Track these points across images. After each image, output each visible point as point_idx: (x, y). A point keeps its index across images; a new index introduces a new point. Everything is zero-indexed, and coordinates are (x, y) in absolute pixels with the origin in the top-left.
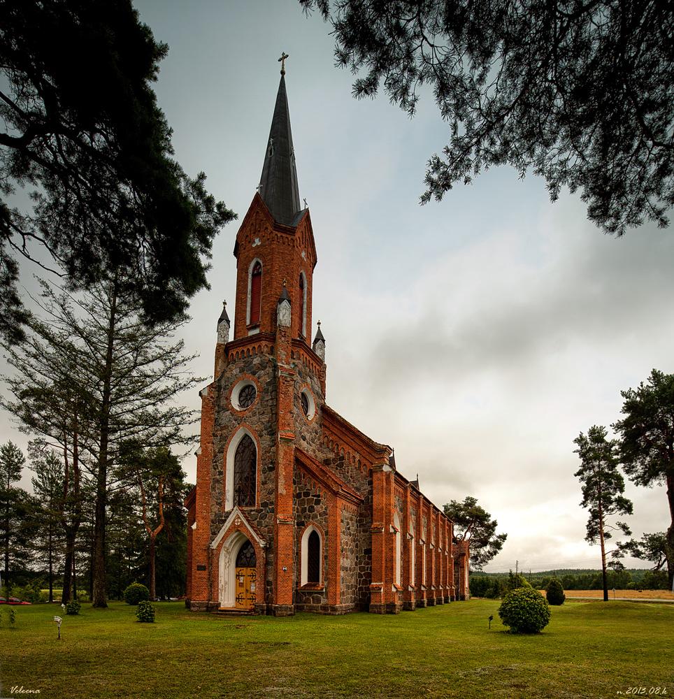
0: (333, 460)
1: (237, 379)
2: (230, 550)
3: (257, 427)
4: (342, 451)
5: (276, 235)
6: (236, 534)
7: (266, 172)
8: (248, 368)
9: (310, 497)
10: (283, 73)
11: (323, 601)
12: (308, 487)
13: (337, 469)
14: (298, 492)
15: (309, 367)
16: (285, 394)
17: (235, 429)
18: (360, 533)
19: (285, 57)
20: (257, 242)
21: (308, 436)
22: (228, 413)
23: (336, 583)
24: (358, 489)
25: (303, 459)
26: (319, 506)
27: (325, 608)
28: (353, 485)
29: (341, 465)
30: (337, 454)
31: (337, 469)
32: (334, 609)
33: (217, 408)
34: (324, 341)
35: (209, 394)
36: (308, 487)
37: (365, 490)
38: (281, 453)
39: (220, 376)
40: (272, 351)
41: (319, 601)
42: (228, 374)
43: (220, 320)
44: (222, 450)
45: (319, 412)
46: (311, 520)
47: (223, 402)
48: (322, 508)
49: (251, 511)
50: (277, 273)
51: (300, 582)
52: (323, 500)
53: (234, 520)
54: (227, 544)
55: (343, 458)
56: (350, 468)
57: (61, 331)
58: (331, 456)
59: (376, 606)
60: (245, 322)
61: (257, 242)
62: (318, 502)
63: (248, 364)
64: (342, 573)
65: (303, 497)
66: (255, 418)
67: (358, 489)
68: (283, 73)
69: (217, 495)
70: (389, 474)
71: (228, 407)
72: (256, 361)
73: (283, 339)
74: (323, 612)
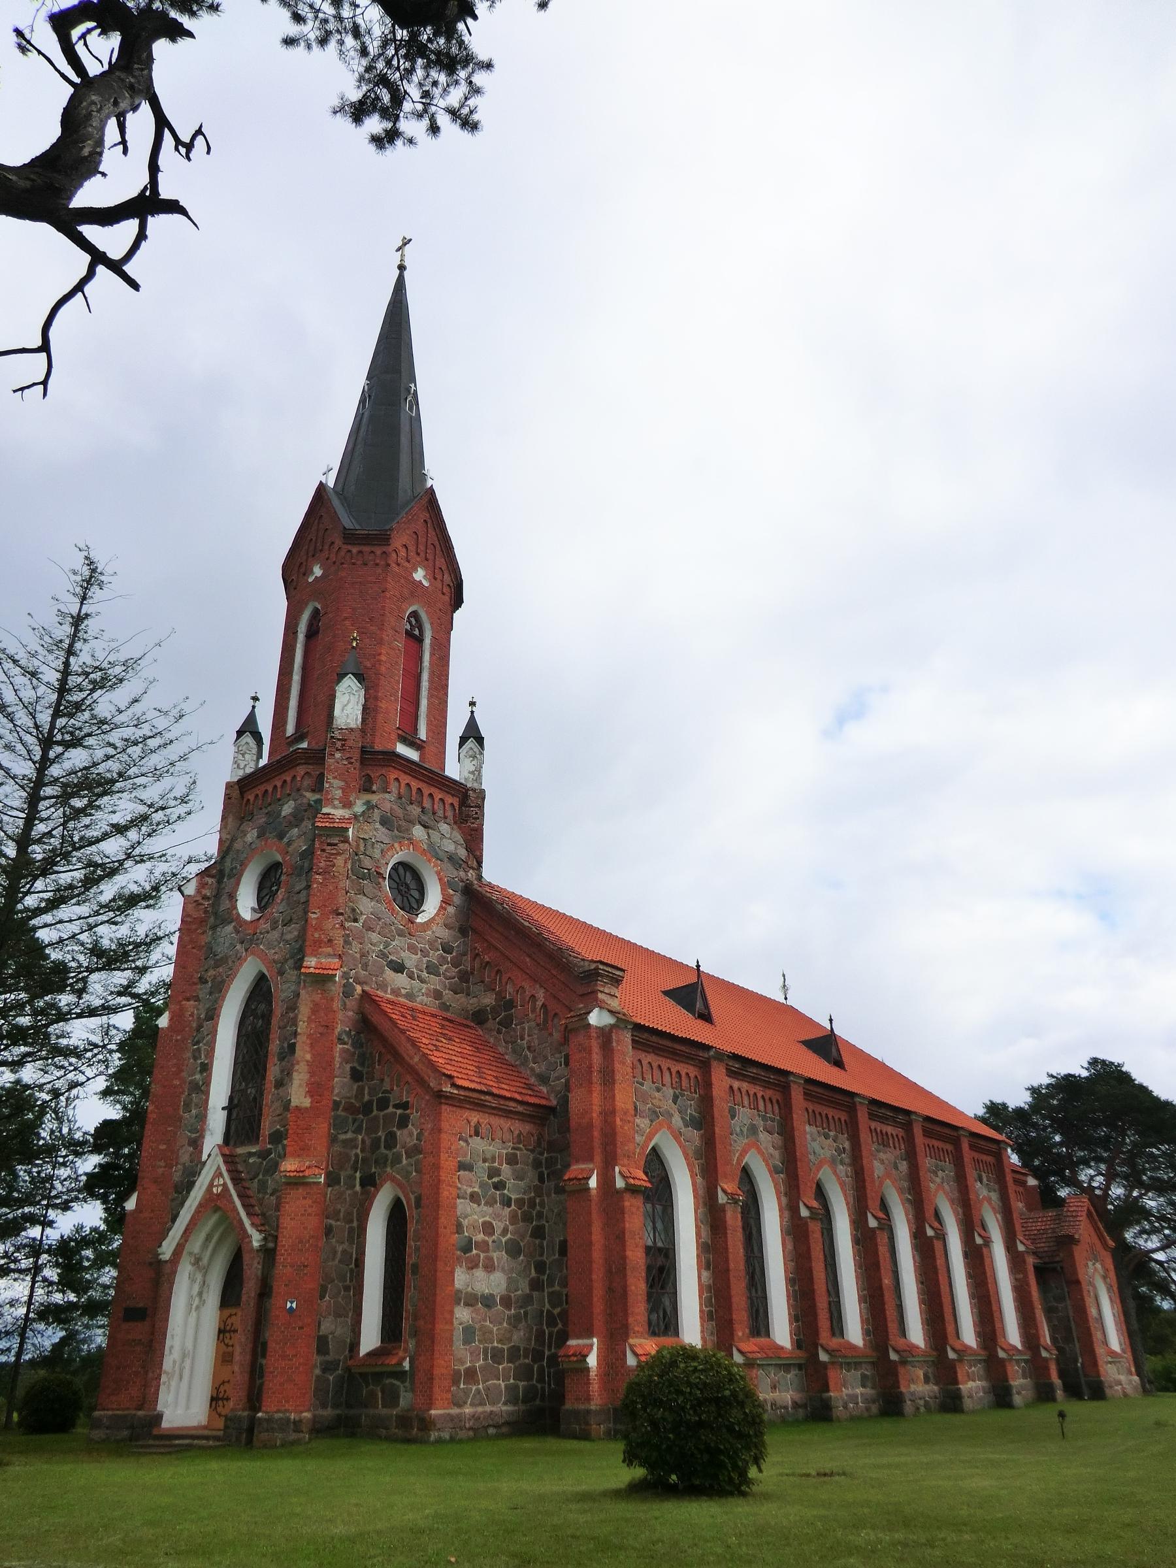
0: (493, 1008)
1: (252, 849)
2: (205, 1260)
3: (274, 954)
4: (510, 988)
5: (349, 551)
6: (214, 1218)
7: (353, 438)
8: (275, 829)
9: (391, 1109)
10: (402, 268)
11: (405, 1399)
12: (387, 1086)
13: (499, 1032)
14: (366, 1098)
15: (420, 803)
16: (325, 872)
17: (240, 960)
18: (549, 1195)
19: (406, 242)
20: (318, 571)
21: (411, 960)
22: (229, 928)
23: (433, 1342)
24: (543, 1079)
25: (376, 1019)
26: (405, 1131)
27: (404, 1421)
28: (532, 1069)
29: (507, 1023)
30: (500, 996)
31: (499, 1032)
32: (426, 1424)
33: (212, 919)
34: (480, 740)
35: (198, 891)
36: (387, 1086)
37: (558, 1078)
38: (304, 1011)
39: (226, 848)
40: (318, 786)
41: (392, 1398)
42: (237, 845)
43: (240, 733)
44: (212, 1015)
45: (457, 899)
46: (388, 1169)
47: (225, 904)
48: (411, 1134)
49: (250, 1154)
50: (347, 623)
51: (358, 1344)
52: (414, 1115)
53: (213, 1180)
54: (195, 1245)
55: (510, 1005)
56: (526, 1026)
57: (173, 752)
58: (488, 1000)
59: (576, 1413)
60: (284, 731)
61: (318, 571)
62: (403, 1122)
63: (274, 816)
64: (463, 1314)
65: (375, 1112)
66: (275, 935)
67: (543, 1079)
68: (402, 268)
69: (193, 1121)
70: (611, 1031)
71: (231, 917)
72: (287, 809)
73: (338, 755)
74: (399, 1432)
